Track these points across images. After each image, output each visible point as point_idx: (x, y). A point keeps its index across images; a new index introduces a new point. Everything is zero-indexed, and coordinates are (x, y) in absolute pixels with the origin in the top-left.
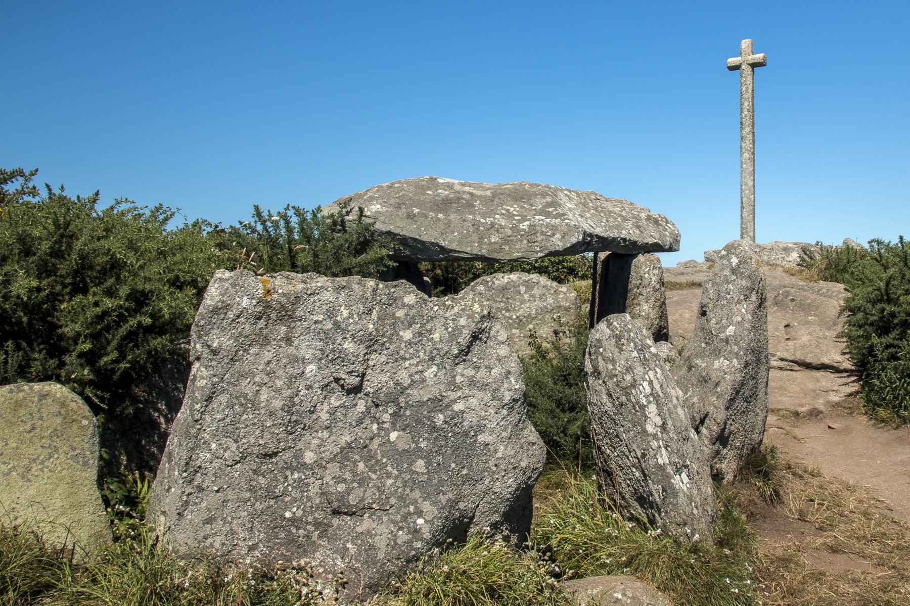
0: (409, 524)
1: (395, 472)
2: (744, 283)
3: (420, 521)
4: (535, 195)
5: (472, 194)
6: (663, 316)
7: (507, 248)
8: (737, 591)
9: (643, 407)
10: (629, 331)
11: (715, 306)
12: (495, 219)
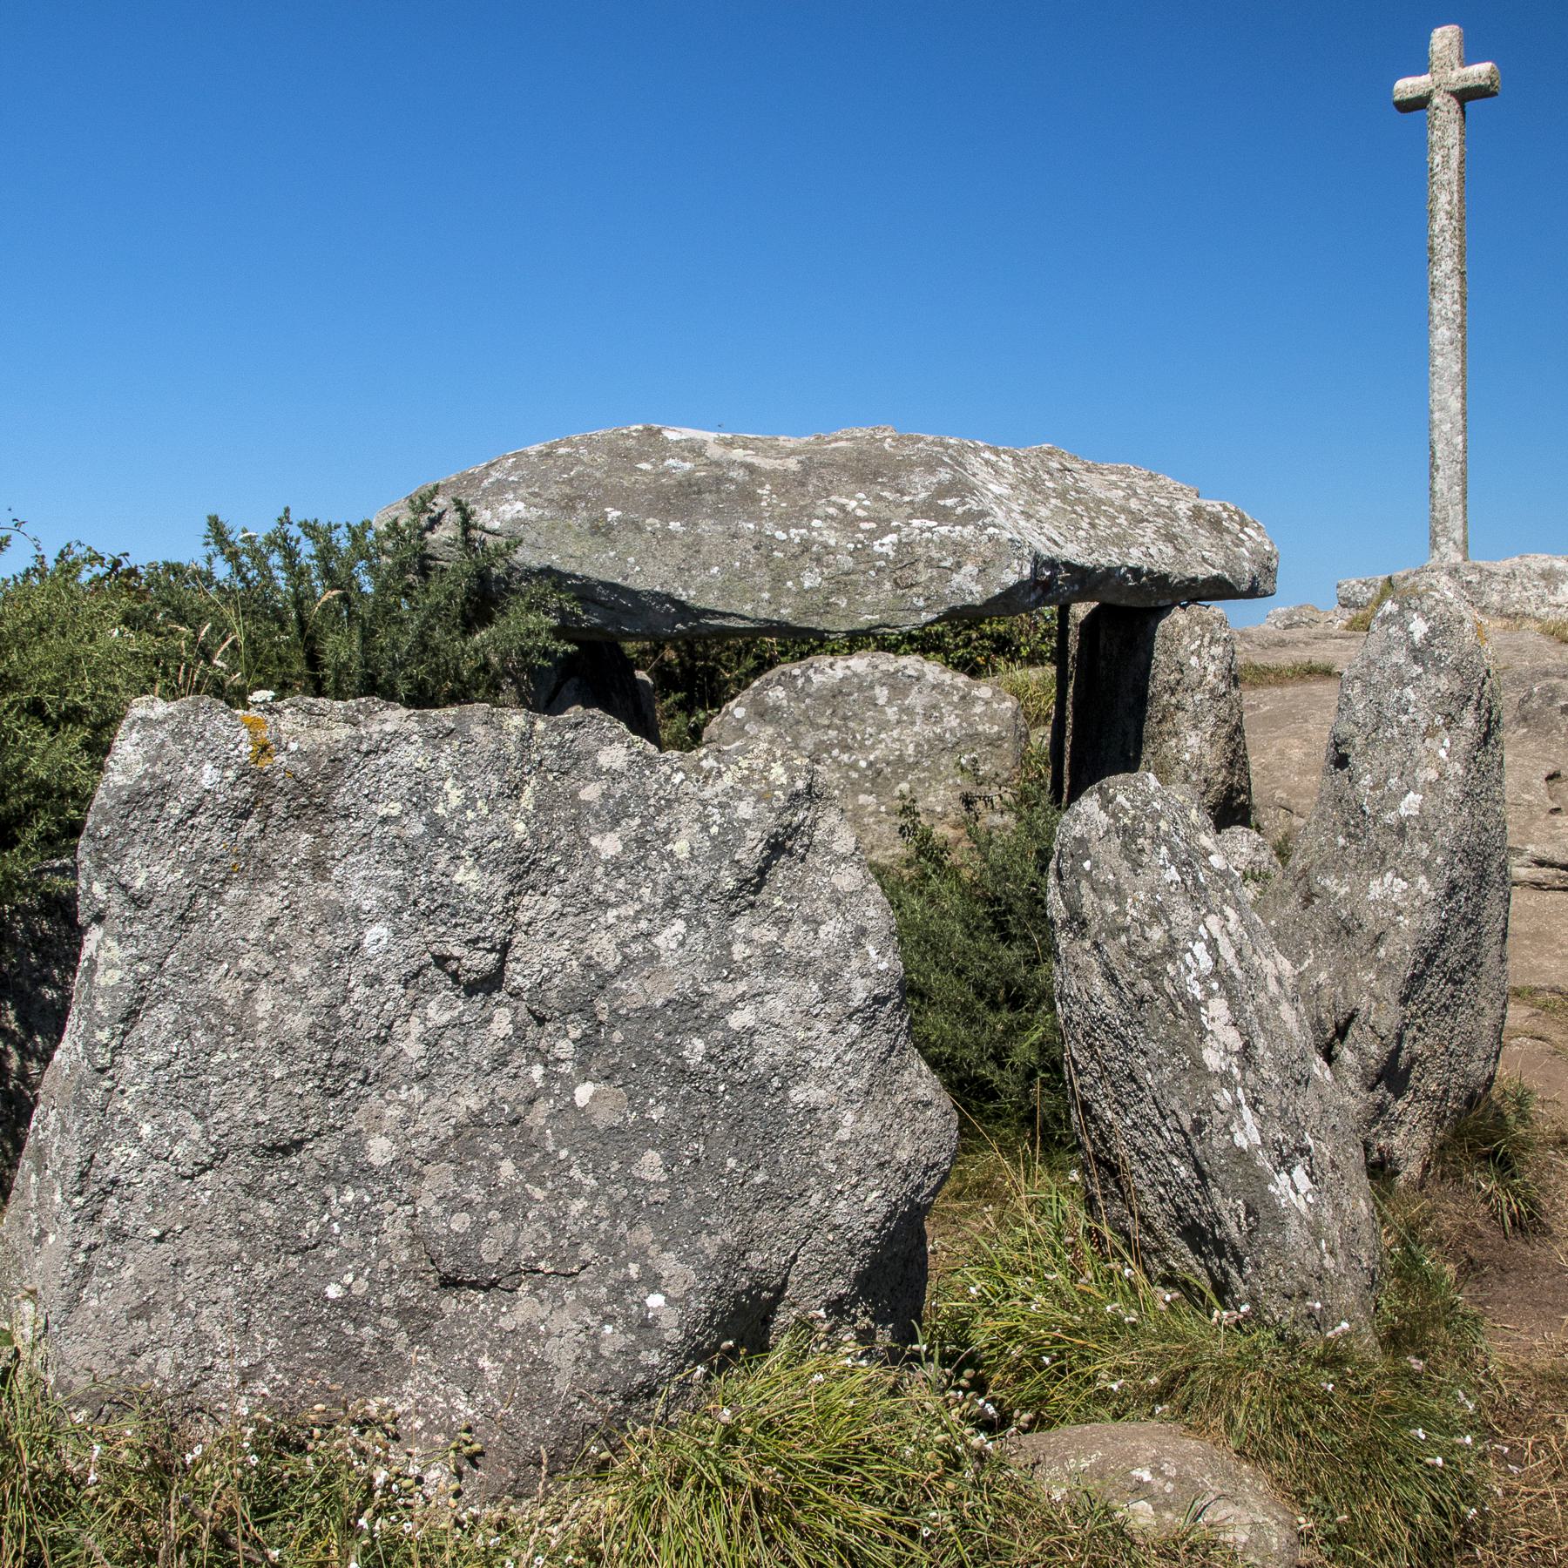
0: (628, 1308)
1: (591, 1182)
2: (1443, 683)
3: (655, 1301)
4: (908, 465)
5: (751, 468)
6: (1236, 760)
7: (843, 603)
8: (1439, 1461)
9: (1193, 1006)
10: (1157, 816)
11: (1370, 743)
12: (810, 529)
